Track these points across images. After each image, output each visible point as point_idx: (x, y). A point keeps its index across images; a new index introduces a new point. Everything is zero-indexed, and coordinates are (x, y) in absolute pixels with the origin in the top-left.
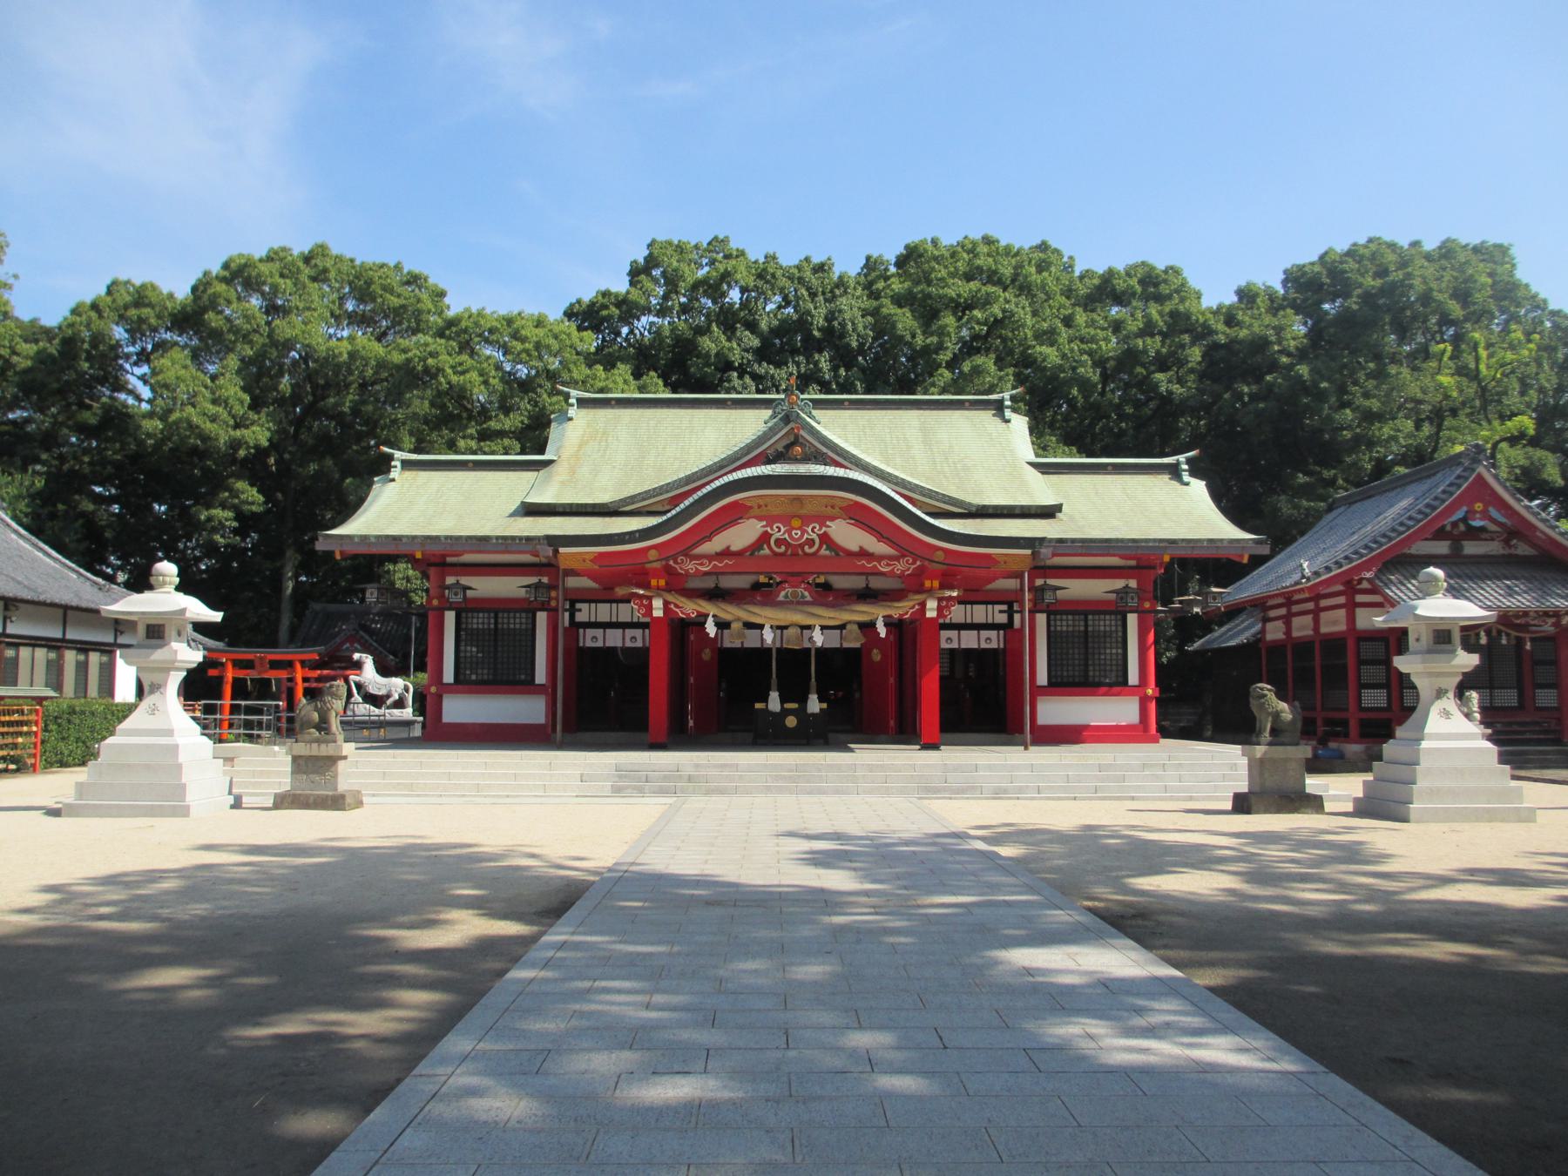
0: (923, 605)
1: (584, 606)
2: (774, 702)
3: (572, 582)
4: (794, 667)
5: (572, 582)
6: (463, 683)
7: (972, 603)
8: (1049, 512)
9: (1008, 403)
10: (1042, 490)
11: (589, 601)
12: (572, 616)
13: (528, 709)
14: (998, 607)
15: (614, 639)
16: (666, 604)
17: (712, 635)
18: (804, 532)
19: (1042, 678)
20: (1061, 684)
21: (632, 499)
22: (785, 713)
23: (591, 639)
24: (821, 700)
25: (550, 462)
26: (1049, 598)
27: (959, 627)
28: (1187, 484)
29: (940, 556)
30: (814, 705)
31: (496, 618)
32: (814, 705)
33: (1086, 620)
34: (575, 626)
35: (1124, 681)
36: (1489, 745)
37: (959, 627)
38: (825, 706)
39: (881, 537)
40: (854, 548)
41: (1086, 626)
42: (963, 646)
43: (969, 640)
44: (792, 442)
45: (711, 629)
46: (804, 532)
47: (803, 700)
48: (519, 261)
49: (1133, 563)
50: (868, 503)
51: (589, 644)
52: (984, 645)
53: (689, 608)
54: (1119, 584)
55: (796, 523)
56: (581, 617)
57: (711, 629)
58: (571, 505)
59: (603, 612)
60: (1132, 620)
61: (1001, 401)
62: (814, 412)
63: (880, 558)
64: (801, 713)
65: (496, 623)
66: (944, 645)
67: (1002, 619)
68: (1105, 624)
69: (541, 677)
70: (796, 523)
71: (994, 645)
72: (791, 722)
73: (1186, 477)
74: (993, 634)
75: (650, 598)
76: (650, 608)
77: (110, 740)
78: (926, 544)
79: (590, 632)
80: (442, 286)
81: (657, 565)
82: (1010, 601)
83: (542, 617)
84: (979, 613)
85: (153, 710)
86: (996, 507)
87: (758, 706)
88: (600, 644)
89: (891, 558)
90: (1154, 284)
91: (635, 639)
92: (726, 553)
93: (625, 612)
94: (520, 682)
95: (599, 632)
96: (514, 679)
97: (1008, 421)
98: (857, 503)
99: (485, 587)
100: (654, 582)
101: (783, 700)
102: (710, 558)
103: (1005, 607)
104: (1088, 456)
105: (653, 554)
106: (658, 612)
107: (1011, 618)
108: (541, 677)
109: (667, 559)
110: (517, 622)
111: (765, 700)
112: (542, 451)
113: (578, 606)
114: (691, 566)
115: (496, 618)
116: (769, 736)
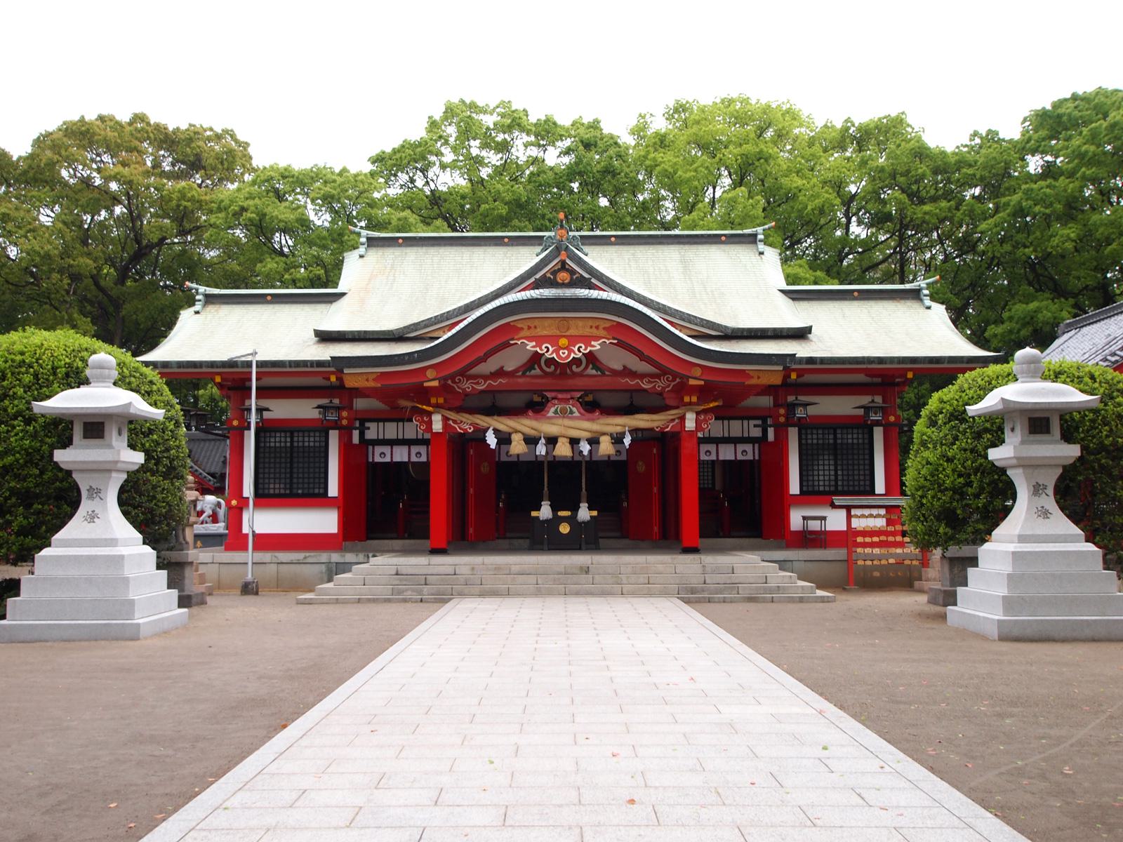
0: (682, 419)
1: (373, 426)
2: (545, 512)
3: (360, 404)
4: (566, 479)
5: (360, 404)
6: (265, 498)
7: (730, 418)
8: (801, 334)
9: (761, 237)
10: (790, 315)
11: (378, 420)
12: (362, 434)
13: (325, 521)
14: (752, 422)
15: (400, 454)
16: (445, 419)
17: (493, 446)
18: (571, 351)
19: (794, 488)
20: (810, 494)
21: (416, 326)
22: (557, 520)
23: (381, 455)
24: (590, 508)
25: (343, 294)
26: (800, 413)
27: (718, 441)
28: (929, 308)
29: (698, 372)
30: (584, 513)
31: (292, 438)
32: (584, 513)
33: (835, 434)
34: (365, 443)
35: (871, 491)
36: (1091, 547)
37: (718, 441)
38: (595, 513)
39: (642, 357)
40: (617, 366)
41: (835, 438)
42: (721, 458)
43: (727, 453)
44: (562, 270)
45: (492, 440)
46: (571, 351)
47: (575, 509)
48: (306, 115)
49: (878, 380)
50: (629, 322)
51: (378, 459)
52: (740, 457)
53: (466, 423)
54: (865, 400)
55: (563, 342)
56: (371, 434)
57: (492, 440)
58: (359, 332)
59: (391, 430)
60: (878, 433)
61: (755, 235)
62: (586, 249)
63: (642, 376)
64: (572, 520)
65: (292, 442)
66: (704, 457)
67: (756, 433)
68: (852, 438)
69: (333, 491)
70: (563, 342)
71: (749, 457)
72: (565, 529)
73: (927, 302)
74: (748, 447)
75: (429, 414)
76: (430, 423)
77: (46, 552)
78: (663, 364)
79: (378, 450)
80: (425, 124)
81: (435, 384)
82: (762, 417)
83: (334, 437)
84: (736, 428)
85: (92, 517)
86: (750, 330)
87: (534, 514)
88: (388, 459)
89: (652, 376)
90: (887, 131)
91: (419, 455)
92: (500, 373)
93: (411, 430)
94: (313, 496)
95: (387, 449)
96: (307, 493)
97: (761, 253)
98: (619, 323)
99: (282, 410)
100: (433, 400)
101: (555, 508)
102: (485, 378)
103: (759, 422)
104: (841, 283)
105: (430, 374)
106: (437, 426)
107: (765, 432)
108: (333, 491)
109: (445, 379)
110: (311, 441)
111: (538, 509)
112: (336, 285)
113: (367, 424)
114: (467, 386)
115: (292, 438)
116: (544, 540)
